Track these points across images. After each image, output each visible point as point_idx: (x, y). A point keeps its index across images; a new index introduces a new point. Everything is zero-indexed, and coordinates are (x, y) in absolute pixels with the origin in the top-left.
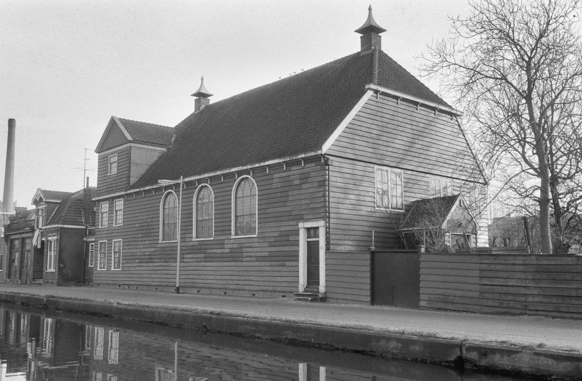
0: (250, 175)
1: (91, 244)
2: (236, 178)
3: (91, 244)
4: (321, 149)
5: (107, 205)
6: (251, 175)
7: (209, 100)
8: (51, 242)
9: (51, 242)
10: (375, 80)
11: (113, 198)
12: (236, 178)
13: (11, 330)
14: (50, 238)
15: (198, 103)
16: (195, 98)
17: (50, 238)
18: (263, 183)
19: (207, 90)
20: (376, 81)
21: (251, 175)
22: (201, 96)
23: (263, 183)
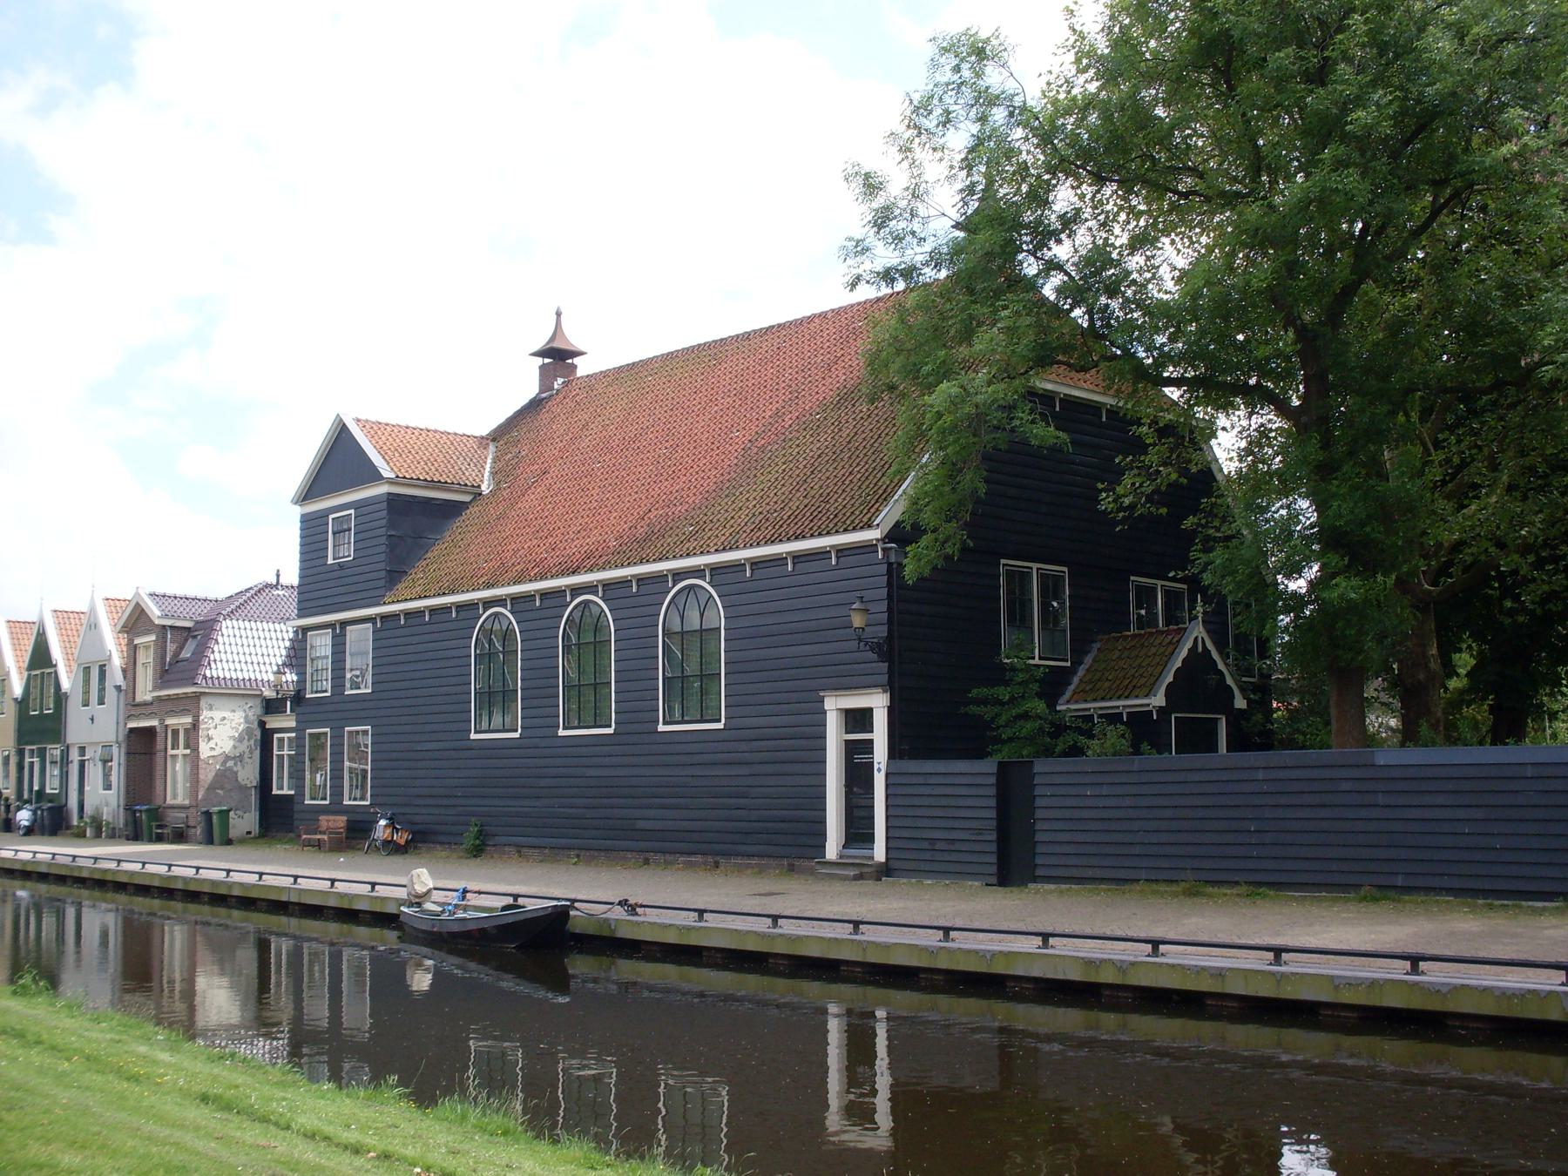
0: (598, 596)
1: (276, 736)
2: (481, 612)
3: (276, 736)
4: (1056, 449)
5: (328, 640)
6: (509, 607)
7: (574, 367)
8: (176, 733)
9: (176, 733)
10: (1028, 239)
11: (344, 624)
12: (481, 612)
13: (1188, 413)
14: (169, 721)
15: (546, 375)
16: (539, 361)
17: (169, 721)
18: (627, 613)
19: (574, 337)
20: (1024, 238)
21: (509, 607)
22: (557, 357)
23: (627, 613)
